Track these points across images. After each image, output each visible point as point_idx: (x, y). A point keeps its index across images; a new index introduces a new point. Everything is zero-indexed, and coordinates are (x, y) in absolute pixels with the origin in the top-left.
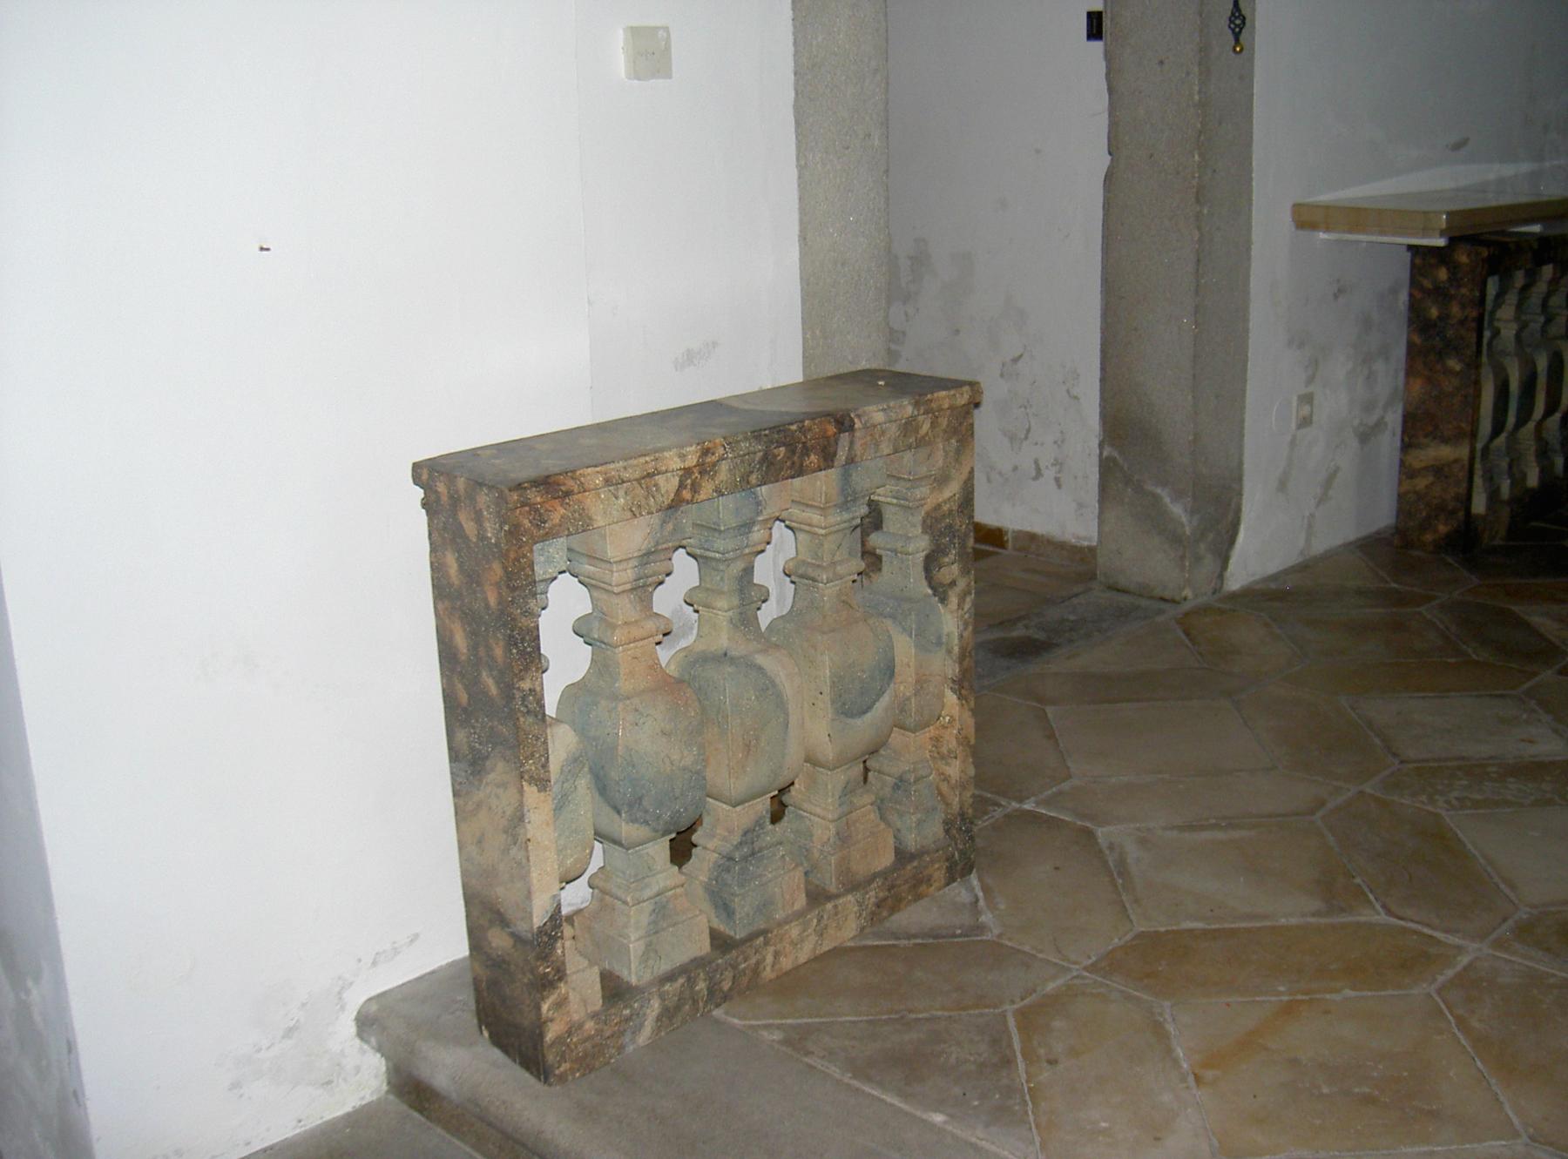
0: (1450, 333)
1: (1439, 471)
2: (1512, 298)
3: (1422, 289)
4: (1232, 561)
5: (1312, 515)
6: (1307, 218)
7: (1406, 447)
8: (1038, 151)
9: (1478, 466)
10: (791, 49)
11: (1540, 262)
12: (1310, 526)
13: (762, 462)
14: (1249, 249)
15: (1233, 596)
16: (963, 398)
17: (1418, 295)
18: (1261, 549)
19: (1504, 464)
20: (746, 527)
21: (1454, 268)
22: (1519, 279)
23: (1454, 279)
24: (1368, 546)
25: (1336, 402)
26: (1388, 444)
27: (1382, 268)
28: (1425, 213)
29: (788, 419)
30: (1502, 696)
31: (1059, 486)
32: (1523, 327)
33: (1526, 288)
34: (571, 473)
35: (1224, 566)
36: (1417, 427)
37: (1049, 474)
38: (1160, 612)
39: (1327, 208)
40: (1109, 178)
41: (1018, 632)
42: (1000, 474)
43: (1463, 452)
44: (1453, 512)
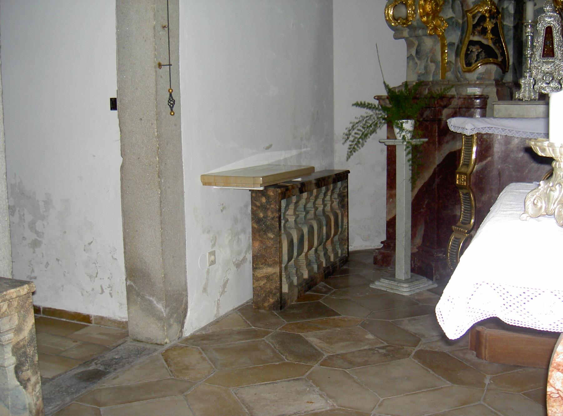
0: (268, 223)
1: (268, 278)
2: (292, 207)
3: (256, 206)
5: (219, 300)
6: (208, 181)
7: (254, 269)
8: (94, 156)
9: (283, 273)
11: (301, 191)
12: (218, 304)
14: (183, 195)
15: (187, 339)
17: (255, 208)
18: (197, 319)
19: (294, 271)
21: (268, 197)
22: (294, 199)
23: (268, 202)
24: (243, 309)
25: (224, 253)
26: (248, 266)
27: (240, 199)
28: (253, 177)
30: (297, 379)
31: (112, 297)
32: (297, 216)
33: (297, 203)
35: (182, 327)
36: (258, 260)
37: (107, 291)
38: (155, 350)
39: (215, 176)
40: (122, 167)
41: (92, 367)
42: (87, 292)
43: (277, 270)
44: (275, 294)
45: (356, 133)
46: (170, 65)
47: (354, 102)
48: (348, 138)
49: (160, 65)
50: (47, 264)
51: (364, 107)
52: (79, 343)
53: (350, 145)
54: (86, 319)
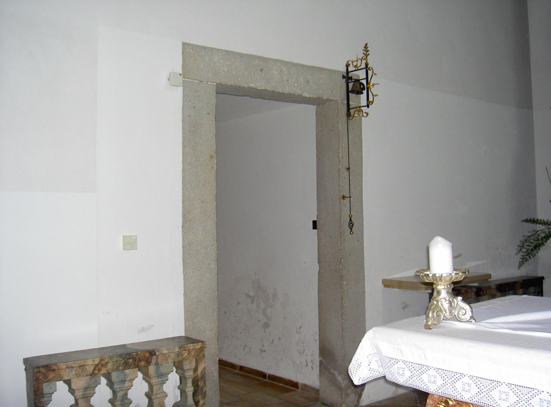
4: (363, 397)
6: (388, 284)
10: (181, 240)
13: (124, 363)
16: (199, 346)
20: (124, 381)
29: (132, 351)
34: (56, 364)
45: (528, 246)
46: (350, 197)
47: (525, 218)
48: (521, 249)
49: (344, 197)
50: (273, 341)
51: (533, 223)
52: (282, 401)
53: (523, 256)
54: (295, 385)
